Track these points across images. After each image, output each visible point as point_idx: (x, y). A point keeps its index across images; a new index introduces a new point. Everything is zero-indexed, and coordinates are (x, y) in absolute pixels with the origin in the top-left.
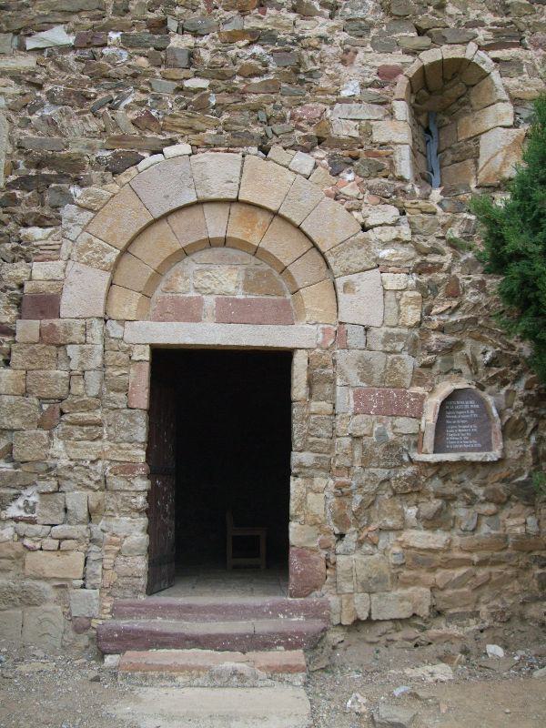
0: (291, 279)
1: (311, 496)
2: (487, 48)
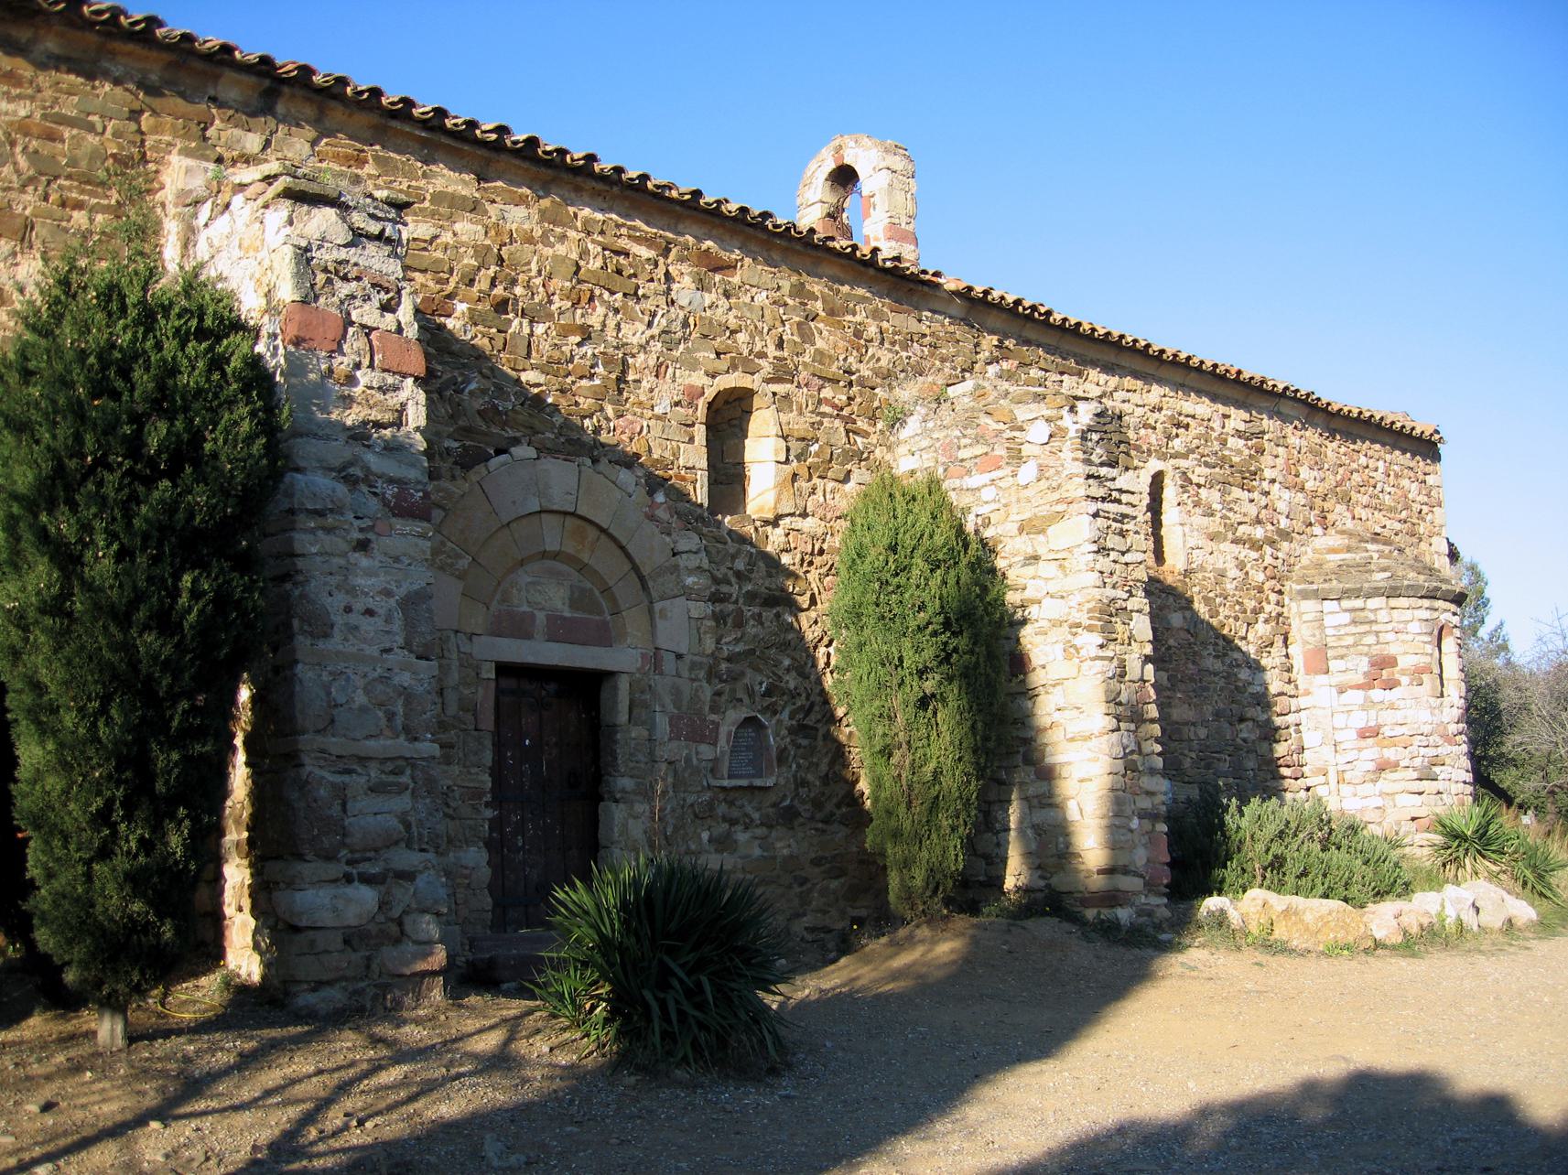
0: (614, 600)
1: (631, 821)
2: (768, 381)
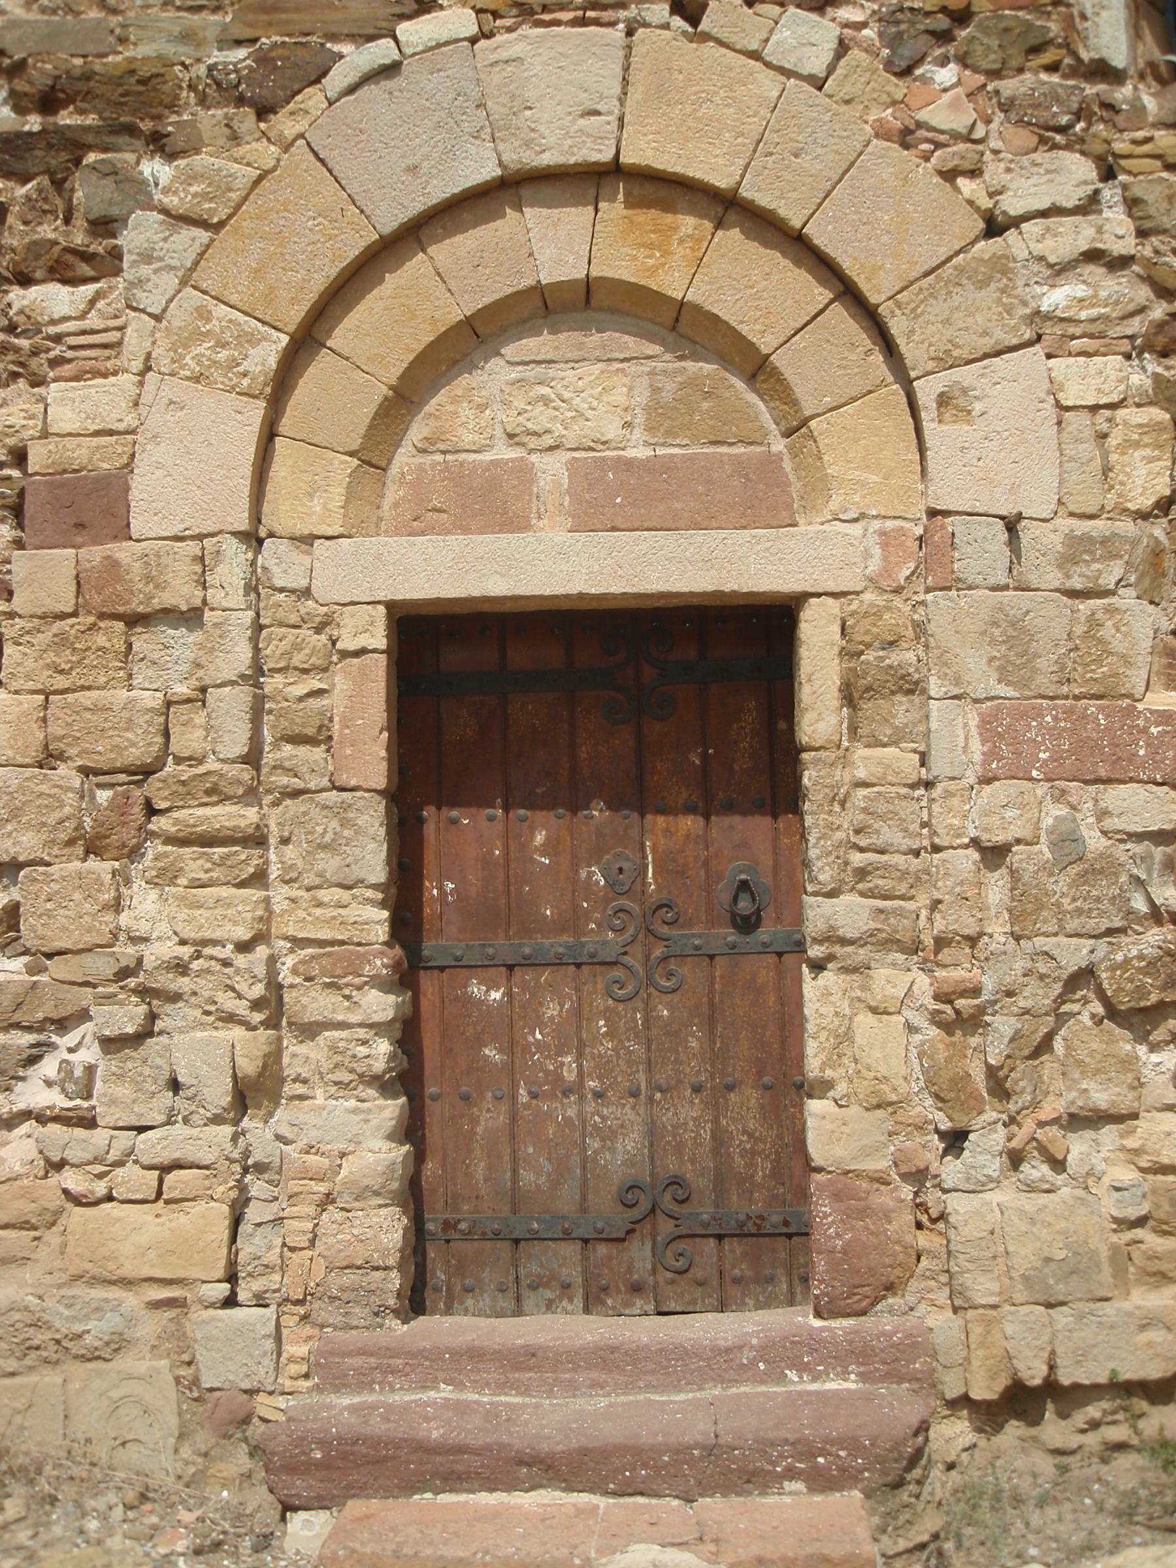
1: (865, 1020)
